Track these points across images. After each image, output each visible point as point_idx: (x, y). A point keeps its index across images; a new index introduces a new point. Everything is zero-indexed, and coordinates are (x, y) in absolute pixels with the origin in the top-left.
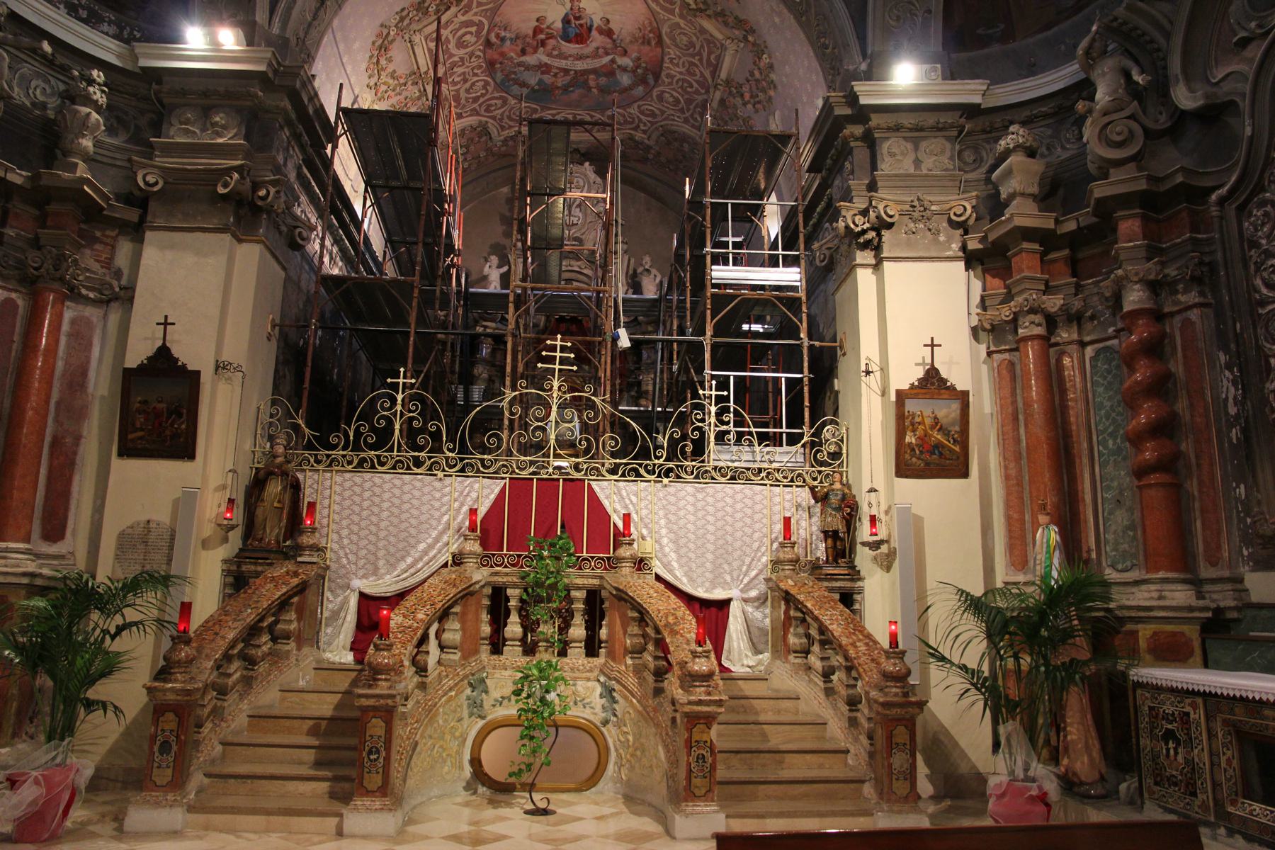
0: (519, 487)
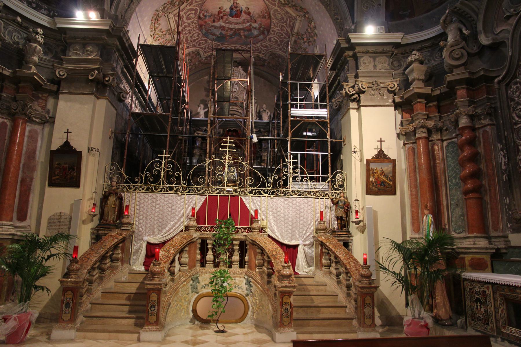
0: (212, 199)
